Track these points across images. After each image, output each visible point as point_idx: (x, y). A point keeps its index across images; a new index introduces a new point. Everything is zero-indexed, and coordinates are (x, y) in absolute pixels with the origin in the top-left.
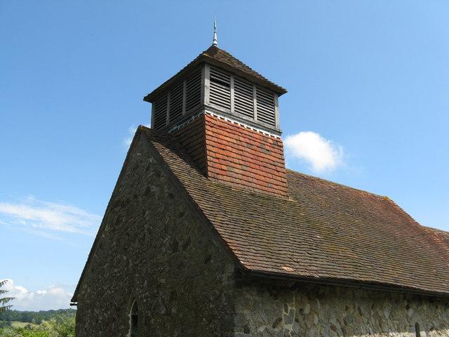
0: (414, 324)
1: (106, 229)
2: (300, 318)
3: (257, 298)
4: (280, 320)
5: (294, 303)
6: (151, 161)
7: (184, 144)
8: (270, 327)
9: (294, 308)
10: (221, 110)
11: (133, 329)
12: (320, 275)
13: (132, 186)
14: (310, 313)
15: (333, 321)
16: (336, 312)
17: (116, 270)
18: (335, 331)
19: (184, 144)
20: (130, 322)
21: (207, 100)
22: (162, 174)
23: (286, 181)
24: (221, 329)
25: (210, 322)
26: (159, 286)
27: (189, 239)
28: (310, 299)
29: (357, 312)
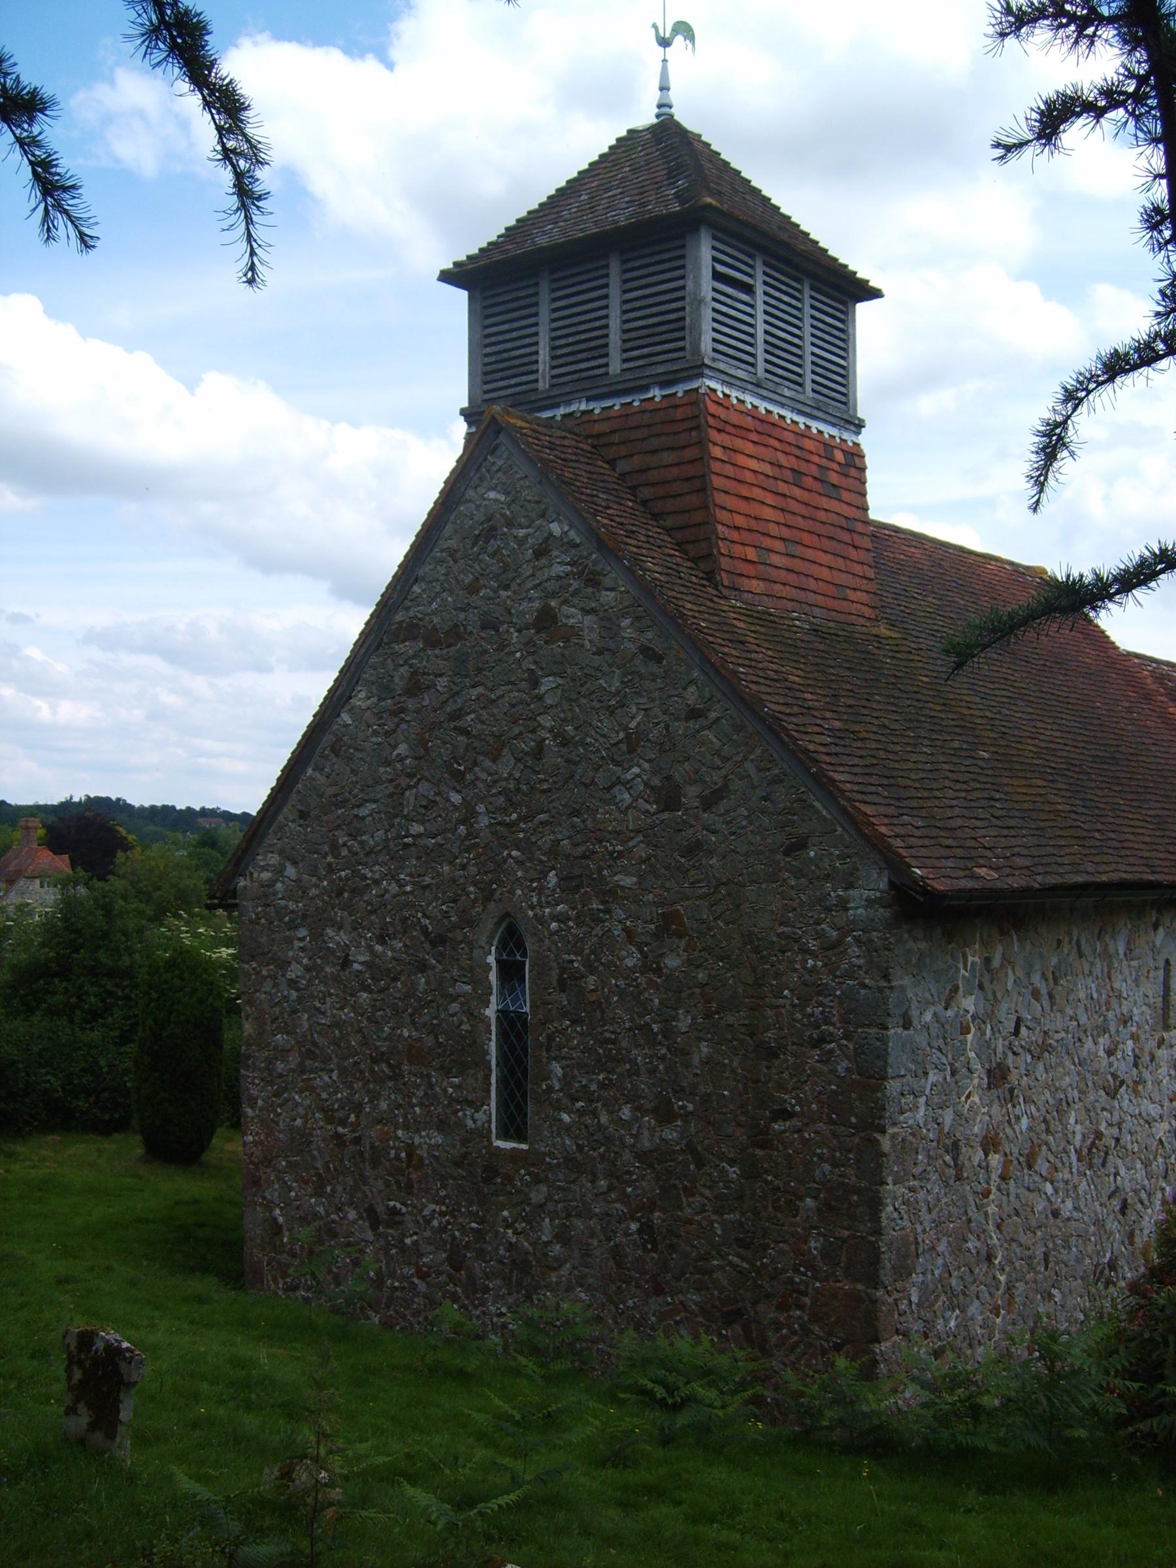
0: (1161, 964)
1: (361, 699)
2: (986, 981)
3: (923, 945)
4: (955, 989)
5: (977, 946)
6: (556, 528)
7: (622, 466)
8: (939, 1008)
9: (977, 959)
10: (732, 372)
11: (502, 996)
12: (1039, 878)
13: (473, 589)
14: (1002, 966)
15: (1036, 979)
16: (1041, 956)
17: (417, 828)
18: (1037, 1000)
19: (622, 466)
20: (493, 976)
21: (706, 345)
22: (607, 582)
23: (870, 573)
24: (845, 1021)
25: (805, 1000)
26: (610, 895)
27: (725, 786)
28: (1002, 933)
29: (1075, 950)
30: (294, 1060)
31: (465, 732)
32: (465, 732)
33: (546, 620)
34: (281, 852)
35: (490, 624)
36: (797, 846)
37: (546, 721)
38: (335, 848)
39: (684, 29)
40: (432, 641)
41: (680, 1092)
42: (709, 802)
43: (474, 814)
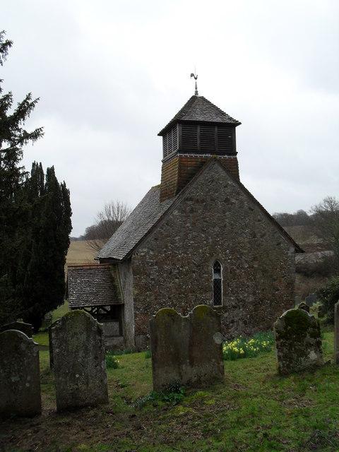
17: (192, 242)
30: (153, 297)
31: (206, 222)
32: (206, 222)
33: (227, 200)
34: (148, 248)
35: (213, 200)
36: (279, 244)
37: (227, 220)
38: (166, 247)
39: (192, 75)
40: (197, 201)
41: (257, 289)
42: (262, 237)
43: (208, 238)
